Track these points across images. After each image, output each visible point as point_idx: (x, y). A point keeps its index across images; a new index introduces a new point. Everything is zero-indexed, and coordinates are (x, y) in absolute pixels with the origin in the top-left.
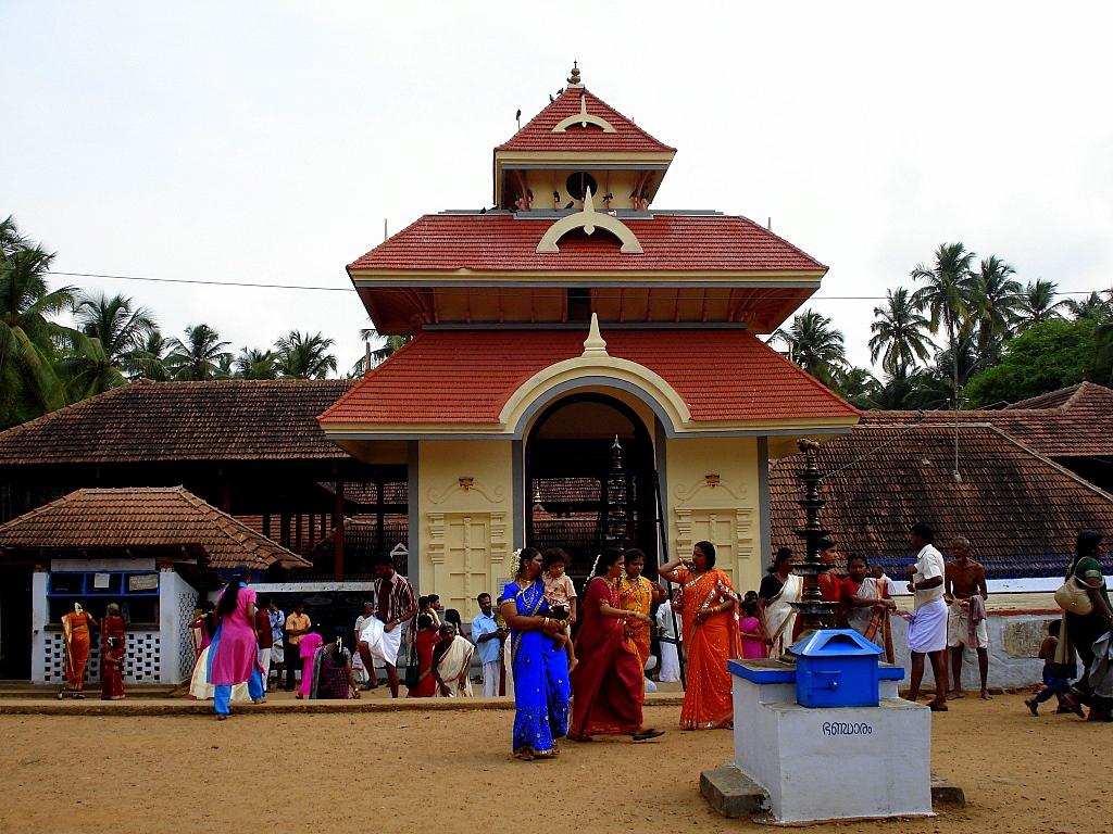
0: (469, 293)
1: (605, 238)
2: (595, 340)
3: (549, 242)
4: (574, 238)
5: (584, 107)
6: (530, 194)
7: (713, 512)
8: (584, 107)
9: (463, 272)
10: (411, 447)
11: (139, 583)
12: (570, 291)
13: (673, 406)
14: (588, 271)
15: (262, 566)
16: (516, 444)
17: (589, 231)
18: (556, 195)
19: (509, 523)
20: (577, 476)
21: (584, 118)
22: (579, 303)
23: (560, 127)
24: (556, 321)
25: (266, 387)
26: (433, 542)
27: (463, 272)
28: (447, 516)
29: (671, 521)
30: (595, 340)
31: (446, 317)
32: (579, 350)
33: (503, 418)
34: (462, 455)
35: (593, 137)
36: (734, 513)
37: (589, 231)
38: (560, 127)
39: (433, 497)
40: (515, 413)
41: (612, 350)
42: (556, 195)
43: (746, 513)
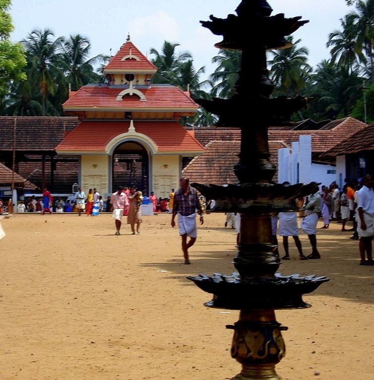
0: (96, 113)
1: (136, 97)
2: (132, 128)
3: (119, 98)
4: (127, 97)
5: (130, 52)
6: (114, 80)
7: (166, 176)
8: (130, 52)
9: (95, 107)
10: (79, 156)
11: (6, 193)
12: (126, 112)
13: (153, 146)
14: (131, 106)
15: (33, 189)
16: (109, 156)
17: (131, 94)
18: (122, 80)
19: (107, 178)
20: (236, 49)
21: (131, 56)
22: (128, 115)
23: (123, 59)
24: (120, 121)
25: (10, 120)
26: (156, 183)
27: (95, 107)
28: (90, 175)
29: (153, 178)
30: (132, 128)
31: (89, 117)
32: (127, 131)
33: (106, 149)
34: (94, 159)
35: (133, 63)
36: (172, 176)
37: (131, 94)
38: (123, 59)
39: (86, 170)
40: (109, 148)
41: (137, 131)
42: (122, 80)
43: (175, 176)
